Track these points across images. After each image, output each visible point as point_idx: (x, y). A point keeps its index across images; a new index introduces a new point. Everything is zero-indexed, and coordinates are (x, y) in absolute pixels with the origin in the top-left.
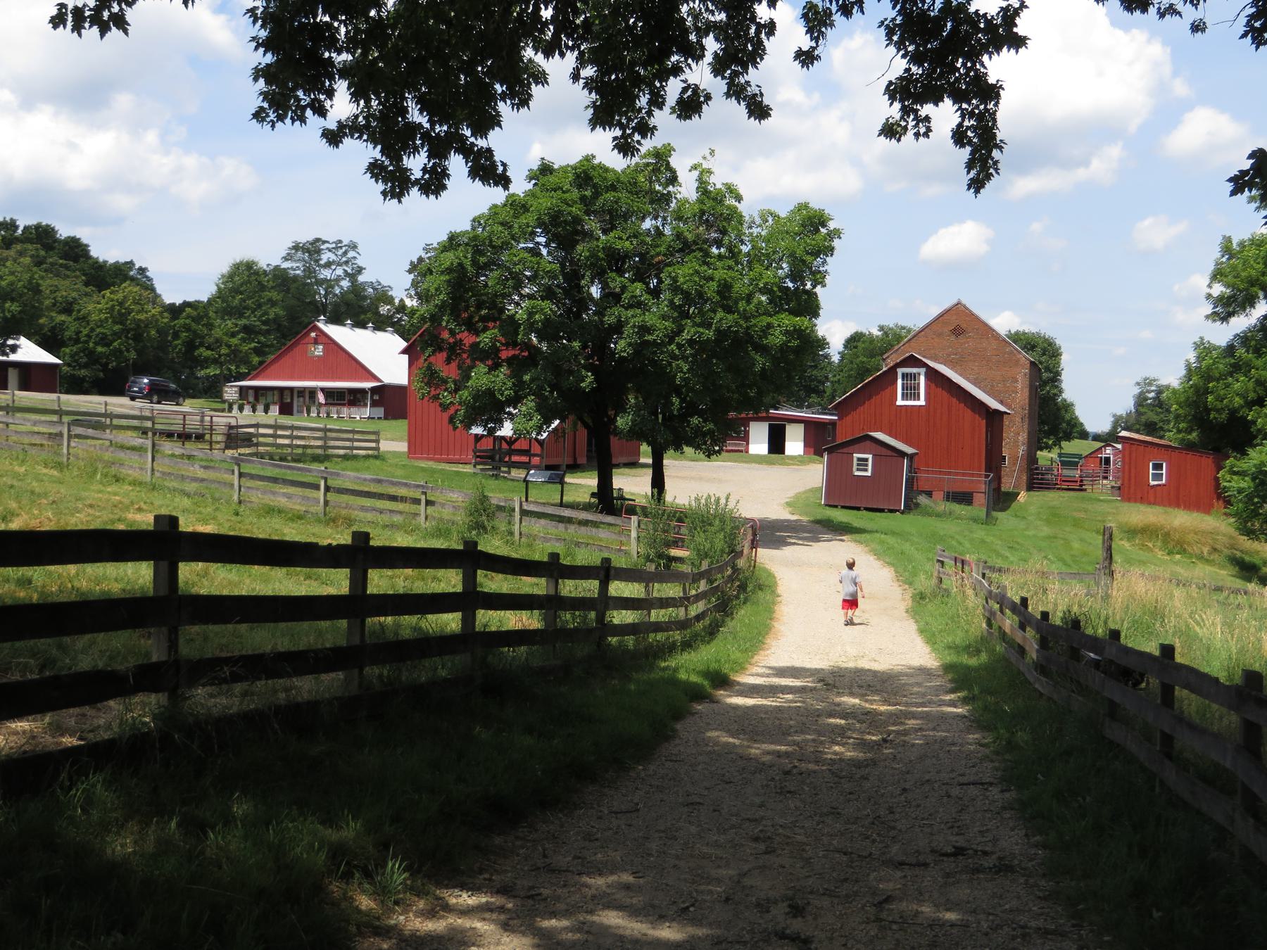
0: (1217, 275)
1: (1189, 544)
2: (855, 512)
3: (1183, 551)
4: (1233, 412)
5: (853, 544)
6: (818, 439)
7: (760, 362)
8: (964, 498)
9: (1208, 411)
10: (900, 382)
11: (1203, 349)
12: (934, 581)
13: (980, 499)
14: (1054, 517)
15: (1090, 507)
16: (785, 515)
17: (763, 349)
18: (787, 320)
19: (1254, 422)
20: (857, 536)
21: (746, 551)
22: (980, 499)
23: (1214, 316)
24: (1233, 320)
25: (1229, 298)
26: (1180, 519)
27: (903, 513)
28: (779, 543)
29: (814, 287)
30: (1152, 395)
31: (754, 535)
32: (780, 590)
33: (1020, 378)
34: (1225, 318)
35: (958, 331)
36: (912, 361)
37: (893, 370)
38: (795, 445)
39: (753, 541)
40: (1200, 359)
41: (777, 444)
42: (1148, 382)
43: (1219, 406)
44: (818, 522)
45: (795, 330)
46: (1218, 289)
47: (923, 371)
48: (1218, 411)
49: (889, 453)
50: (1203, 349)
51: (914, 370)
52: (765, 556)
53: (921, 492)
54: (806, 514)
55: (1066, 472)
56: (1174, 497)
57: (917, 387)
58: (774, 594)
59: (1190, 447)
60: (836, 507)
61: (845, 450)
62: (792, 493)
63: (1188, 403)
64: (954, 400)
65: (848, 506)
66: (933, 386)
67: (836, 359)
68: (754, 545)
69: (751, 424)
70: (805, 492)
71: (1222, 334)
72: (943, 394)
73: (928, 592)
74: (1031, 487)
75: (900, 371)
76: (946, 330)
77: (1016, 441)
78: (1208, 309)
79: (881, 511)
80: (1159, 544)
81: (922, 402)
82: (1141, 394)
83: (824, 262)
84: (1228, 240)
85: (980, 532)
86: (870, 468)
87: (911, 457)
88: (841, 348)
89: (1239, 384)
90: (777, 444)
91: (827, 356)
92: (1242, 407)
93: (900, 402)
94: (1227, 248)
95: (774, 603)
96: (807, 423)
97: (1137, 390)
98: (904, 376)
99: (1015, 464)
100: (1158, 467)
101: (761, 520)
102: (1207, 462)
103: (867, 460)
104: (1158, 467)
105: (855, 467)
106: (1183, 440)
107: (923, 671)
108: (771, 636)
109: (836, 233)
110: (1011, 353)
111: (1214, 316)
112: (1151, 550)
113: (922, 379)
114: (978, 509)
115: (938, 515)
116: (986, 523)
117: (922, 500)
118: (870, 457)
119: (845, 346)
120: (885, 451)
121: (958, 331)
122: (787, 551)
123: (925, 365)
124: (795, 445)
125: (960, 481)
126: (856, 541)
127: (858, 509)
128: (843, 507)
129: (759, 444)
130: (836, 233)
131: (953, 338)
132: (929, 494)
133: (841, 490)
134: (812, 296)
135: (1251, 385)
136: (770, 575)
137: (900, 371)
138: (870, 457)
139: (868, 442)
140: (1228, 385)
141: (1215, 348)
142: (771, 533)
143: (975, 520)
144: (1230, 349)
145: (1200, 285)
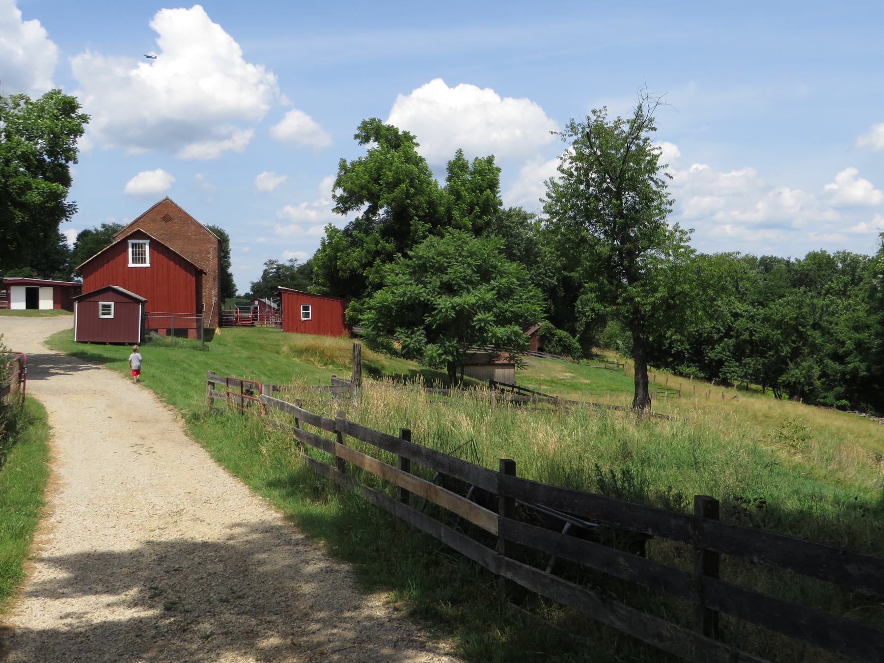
0: (338, 184)
1: (337, 357)
2: (102, 346)
3: (333, 363)
4: (353, 271)
5: (108, 372)
6: (64, 302)
7: (19, 216)
8: (182, 333)
9: (337, 271)
10: (130, 250)
11: (332, 232)
12: (206, 402)
13: (192, 333)
14: (245, 344)
15: (266, 336)
16: (45, 351)
17: (24, 206)
18: (41, 183)
19: (367, 277)
20: (108, 364)
21: (13, 386)
22: (192, 333)
23: (337, 210)
24: (349, 212)
25: (346, 198)
26: (328, 342)
27: (139, 345)
28: (43, 374)
29: (67, 162)
30: (274, 270)
31: (22, 369)
32: (51, 421)
33: (211, 251)
34: (344, 211)
35: (167, 219)
36: (138, 235)
37: (124, 243)
38: (46, 303)
39: (20, 376)
40: (330, 237)
41: (32, 302)
42: (272, 262)
43: (344, 267)
44: (74, 355)
45: (51, 193)
46: (339, 192)
47: (147, 241)
48: (343, 271)
49: (128, 300)
50: (332, 232)
51: (141, 241)
52: (32, 386)
53: (151, 330)
54: (62, 349)
55: (244, 315)
56: (317, 328)
57: (143, 254)
58: (47, 427)
59: (324, 295)
60: (86, 343)
61: (92, 299)
62: (48, 335)
63: (324, 266)
64: (172, 263)
65: (95, 345)
66: (155, 252)
67: (72, 247)
68: (21, 378)
69: (12, 288)
70: (59, 333)
71: (342, 221)
72: (164, 259)
73: (201, 412)
74: (221, 325)
75: (130, 242)
76: (158, 218)
77: (210, 294)
78: (334, 204)
79: (123, 344)
80: (317, 358)
81: (148, 264)
82: (265, 271)
83: (74, 142)
84: (344, 161)
85: (201, 357)
86: (112, 312)
87: (143, 303)
88: (75, 241)
89: (356, 253)
90: (32, 302)
91: (65, 246)
92: (358, 268)
93: (131, 265)
94: (343, 166)
95: (47, 438)
96: (56, 287)
97: (265, 267)
98: (133, 245)
99: (210, 310)
100: (306, 308)
101: (27, 355)
102: (337, 304)
103: (109, 306)
104: (306, 308)
105: (100, 312)
106: (320, 290)
107: (268, 529)
108: (51, 487)
109: (84, 118)
110: (205, 234)
111: (337, 210)
112: (312, 363)
113: (147, 248)
114: (192, 340)
115: (167, 346)
116: (203, 350)
117: (153, 334)
118: (112, 304)
119: (78, 239)
120: (124, 299)
121: (167, 219)
122: (52, 382)
123: (148, 238)
124: (46, 303)
125: (176, 319)
126: (110, 368)
127: (104, 344)
128: (92, 343)
129: (18, 303)
130: (84, 118)
131: (163, 223)
132: (156, 331)
133: (89, 330)
134: (65, 168)
135: (364, 252)
136: (40, 407)
137: (130, 242)
138: (112, 304)
139: (110, 293)
140: (348, 255)
141: (338, 231)
142: (33, 367)
143: (195, 348)
144: (347, 232)
145: (327, 188)
